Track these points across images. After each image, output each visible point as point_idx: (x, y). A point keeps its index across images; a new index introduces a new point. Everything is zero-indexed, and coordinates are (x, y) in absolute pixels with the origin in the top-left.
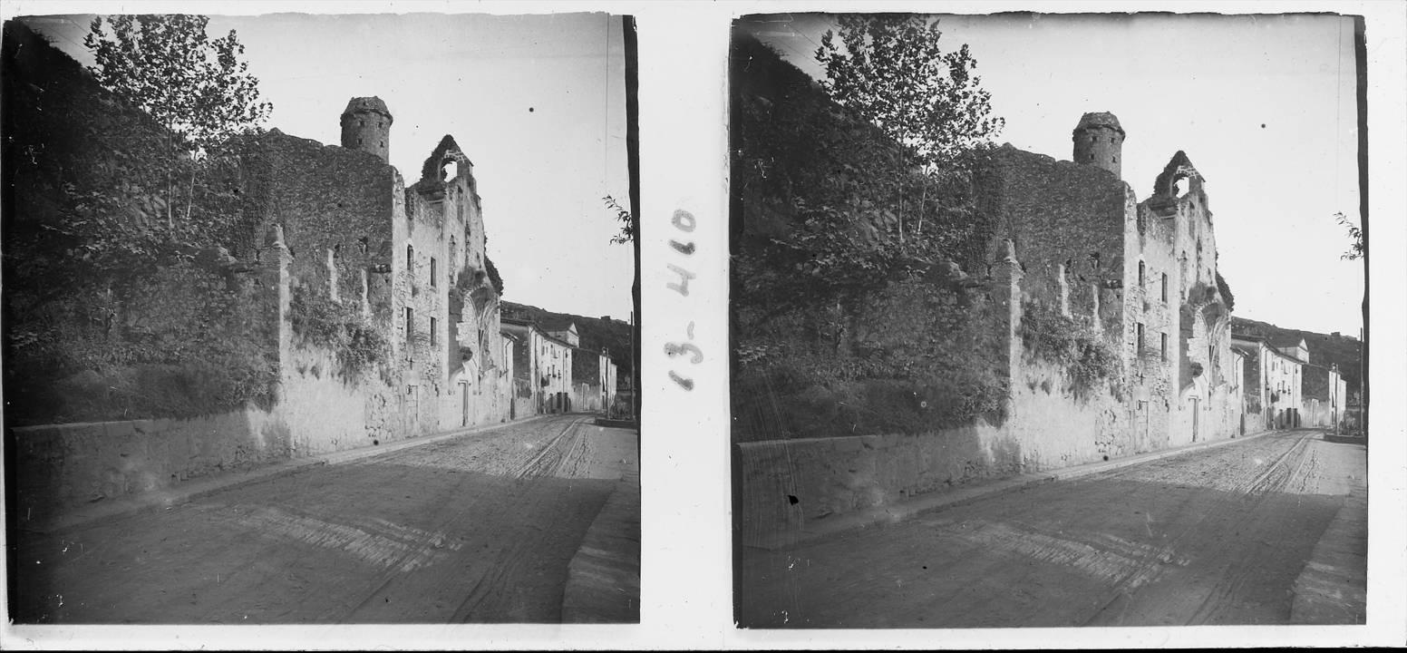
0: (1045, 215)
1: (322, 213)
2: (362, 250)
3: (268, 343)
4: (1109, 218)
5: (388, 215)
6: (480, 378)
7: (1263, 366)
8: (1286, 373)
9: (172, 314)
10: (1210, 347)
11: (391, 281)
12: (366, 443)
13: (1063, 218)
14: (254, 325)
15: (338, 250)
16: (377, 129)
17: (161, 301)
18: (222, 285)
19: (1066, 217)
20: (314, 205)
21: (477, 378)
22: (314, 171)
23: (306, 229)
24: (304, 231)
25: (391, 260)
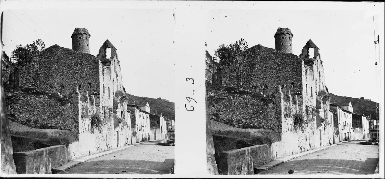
0: (71, 70)
1: (277, 74)
2: (89, 87)
3: (278, 122)
4: (297, 71)
5: (301, 76)
6: (325, 128)
7: (136, 117)
8: (346, 118)
9: (42, 113)
10: (324, 111)
11: (100, 98)
12: (96, 153)
13: (281, 70)
14: (71, 117)
15: (80, 87)
16: (288, 40)
17: (241, 109)
18: (59, 103)
19: (79, 70)
20: (71, 71)
21: (324, 128)
22: (274, 59)
23: (69, 80)
24: (271, 80)
25: (302, 91)
